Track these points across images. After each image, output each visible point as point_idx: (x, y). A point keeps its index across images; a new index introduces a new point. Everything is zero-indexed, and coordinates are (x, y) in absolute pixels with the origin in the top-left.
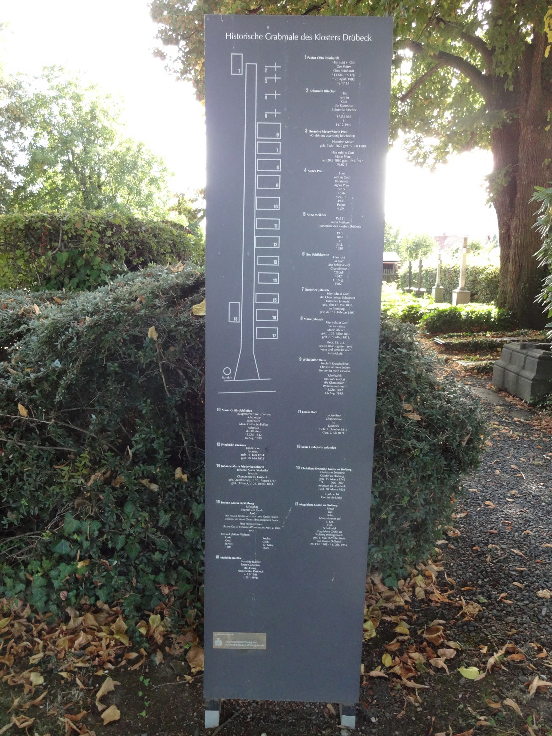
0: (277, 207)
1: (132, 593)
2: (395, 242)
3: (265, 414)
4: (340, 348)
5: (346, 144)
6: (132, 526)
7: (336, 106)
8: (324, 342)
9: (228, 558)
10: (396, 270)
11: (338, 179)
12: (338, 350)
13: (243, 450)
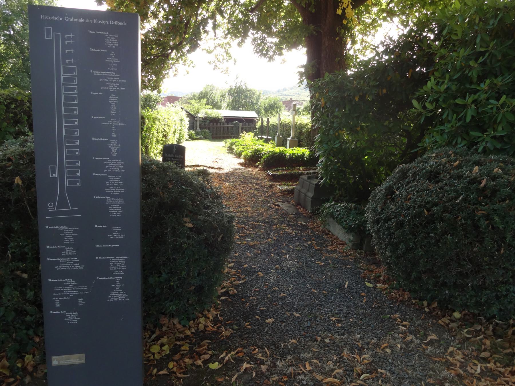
0: (76, 113)
1: (13, 343)
2: (257, 104)
3: (76, 229)
4: (117, 190)
5: (115, 79)
6: (9, 301)
7: (108, 59)
8: (108, 187)
9: (58, 312)
10: (256, 124)
11: (111, 98)
12: (116, 192)
13: (64, 250)
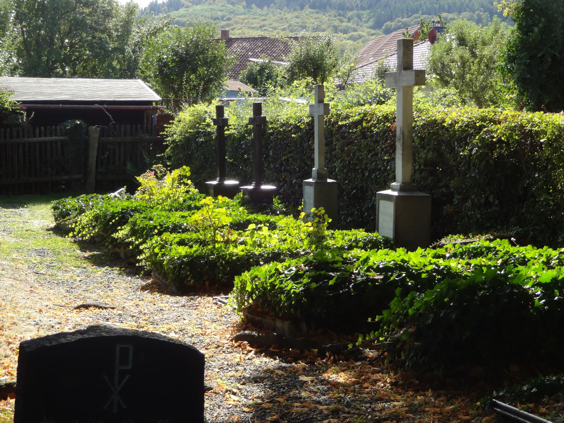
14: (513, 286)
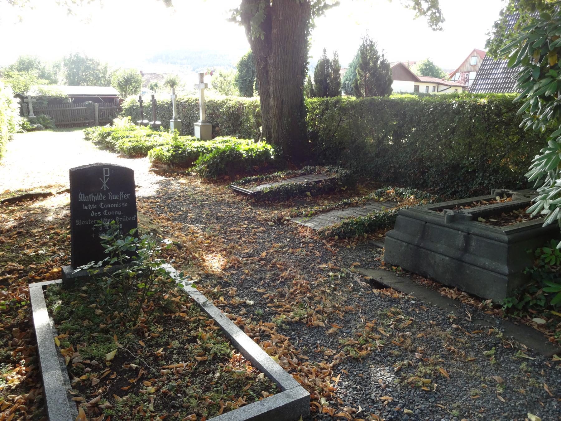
2: (105, 77)
14: (237, 151)
